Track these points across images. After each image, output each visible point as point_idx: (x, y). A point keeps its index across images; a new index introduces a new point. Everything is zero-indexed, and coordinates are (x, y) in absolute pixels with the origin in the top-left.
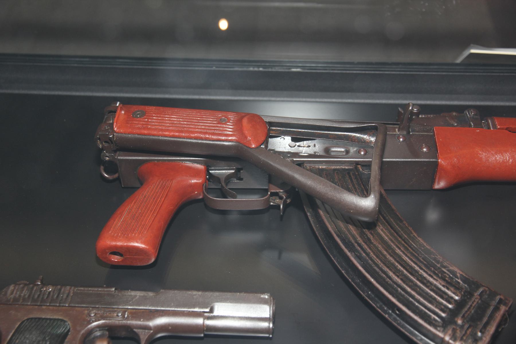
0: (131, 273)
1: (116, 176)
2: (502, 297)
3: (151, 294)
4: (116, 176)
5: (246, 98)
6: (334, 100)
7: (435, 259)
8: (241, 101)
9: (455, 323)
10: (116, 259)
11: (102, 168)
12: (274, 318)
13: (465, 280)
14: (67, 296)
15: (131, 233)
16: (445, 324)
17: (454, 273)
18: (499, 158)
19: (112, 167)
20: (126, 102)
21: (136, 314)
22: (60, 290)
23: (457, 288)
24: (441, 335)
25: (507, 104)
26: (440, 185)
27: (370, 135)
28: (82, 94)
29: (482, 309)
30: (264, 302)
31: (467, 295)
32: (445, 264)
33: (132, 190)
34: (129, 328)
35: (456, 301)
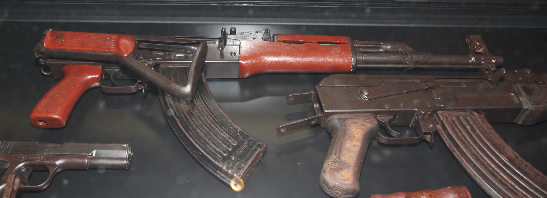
0: (55, 133)
1: (50, 73)
2: (260, 143)
3: (59, 145)
4: (50, 73)
5: (205, 23)
6: (268, 23)
7: (227, 122)
8: (206, 24)
9: (230, 159)
10: (41, 124)
11: (42, 69)
12: (130, 159)
13: (242, 133)
14: (9, 147)
15: (53, 107)
16: (224, 159)
17: (236, 130)
18: (310, 59)
19: (47, 68)
20: (54, 26)
21: (47, 158)
22: (6, 143)
23: (236, 138)
24: (221, 166)
25: (366, 25)
26: (247, 75)
27: (194, 46)
28: (91, 21)
29: (246, 150)
30: (124, 149)
31: (240, 143)
32: (232, 124)
33: (59, 80)
34: (44, 166)
35: (233, 146)
